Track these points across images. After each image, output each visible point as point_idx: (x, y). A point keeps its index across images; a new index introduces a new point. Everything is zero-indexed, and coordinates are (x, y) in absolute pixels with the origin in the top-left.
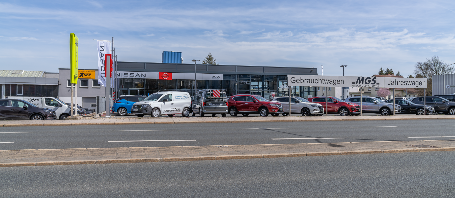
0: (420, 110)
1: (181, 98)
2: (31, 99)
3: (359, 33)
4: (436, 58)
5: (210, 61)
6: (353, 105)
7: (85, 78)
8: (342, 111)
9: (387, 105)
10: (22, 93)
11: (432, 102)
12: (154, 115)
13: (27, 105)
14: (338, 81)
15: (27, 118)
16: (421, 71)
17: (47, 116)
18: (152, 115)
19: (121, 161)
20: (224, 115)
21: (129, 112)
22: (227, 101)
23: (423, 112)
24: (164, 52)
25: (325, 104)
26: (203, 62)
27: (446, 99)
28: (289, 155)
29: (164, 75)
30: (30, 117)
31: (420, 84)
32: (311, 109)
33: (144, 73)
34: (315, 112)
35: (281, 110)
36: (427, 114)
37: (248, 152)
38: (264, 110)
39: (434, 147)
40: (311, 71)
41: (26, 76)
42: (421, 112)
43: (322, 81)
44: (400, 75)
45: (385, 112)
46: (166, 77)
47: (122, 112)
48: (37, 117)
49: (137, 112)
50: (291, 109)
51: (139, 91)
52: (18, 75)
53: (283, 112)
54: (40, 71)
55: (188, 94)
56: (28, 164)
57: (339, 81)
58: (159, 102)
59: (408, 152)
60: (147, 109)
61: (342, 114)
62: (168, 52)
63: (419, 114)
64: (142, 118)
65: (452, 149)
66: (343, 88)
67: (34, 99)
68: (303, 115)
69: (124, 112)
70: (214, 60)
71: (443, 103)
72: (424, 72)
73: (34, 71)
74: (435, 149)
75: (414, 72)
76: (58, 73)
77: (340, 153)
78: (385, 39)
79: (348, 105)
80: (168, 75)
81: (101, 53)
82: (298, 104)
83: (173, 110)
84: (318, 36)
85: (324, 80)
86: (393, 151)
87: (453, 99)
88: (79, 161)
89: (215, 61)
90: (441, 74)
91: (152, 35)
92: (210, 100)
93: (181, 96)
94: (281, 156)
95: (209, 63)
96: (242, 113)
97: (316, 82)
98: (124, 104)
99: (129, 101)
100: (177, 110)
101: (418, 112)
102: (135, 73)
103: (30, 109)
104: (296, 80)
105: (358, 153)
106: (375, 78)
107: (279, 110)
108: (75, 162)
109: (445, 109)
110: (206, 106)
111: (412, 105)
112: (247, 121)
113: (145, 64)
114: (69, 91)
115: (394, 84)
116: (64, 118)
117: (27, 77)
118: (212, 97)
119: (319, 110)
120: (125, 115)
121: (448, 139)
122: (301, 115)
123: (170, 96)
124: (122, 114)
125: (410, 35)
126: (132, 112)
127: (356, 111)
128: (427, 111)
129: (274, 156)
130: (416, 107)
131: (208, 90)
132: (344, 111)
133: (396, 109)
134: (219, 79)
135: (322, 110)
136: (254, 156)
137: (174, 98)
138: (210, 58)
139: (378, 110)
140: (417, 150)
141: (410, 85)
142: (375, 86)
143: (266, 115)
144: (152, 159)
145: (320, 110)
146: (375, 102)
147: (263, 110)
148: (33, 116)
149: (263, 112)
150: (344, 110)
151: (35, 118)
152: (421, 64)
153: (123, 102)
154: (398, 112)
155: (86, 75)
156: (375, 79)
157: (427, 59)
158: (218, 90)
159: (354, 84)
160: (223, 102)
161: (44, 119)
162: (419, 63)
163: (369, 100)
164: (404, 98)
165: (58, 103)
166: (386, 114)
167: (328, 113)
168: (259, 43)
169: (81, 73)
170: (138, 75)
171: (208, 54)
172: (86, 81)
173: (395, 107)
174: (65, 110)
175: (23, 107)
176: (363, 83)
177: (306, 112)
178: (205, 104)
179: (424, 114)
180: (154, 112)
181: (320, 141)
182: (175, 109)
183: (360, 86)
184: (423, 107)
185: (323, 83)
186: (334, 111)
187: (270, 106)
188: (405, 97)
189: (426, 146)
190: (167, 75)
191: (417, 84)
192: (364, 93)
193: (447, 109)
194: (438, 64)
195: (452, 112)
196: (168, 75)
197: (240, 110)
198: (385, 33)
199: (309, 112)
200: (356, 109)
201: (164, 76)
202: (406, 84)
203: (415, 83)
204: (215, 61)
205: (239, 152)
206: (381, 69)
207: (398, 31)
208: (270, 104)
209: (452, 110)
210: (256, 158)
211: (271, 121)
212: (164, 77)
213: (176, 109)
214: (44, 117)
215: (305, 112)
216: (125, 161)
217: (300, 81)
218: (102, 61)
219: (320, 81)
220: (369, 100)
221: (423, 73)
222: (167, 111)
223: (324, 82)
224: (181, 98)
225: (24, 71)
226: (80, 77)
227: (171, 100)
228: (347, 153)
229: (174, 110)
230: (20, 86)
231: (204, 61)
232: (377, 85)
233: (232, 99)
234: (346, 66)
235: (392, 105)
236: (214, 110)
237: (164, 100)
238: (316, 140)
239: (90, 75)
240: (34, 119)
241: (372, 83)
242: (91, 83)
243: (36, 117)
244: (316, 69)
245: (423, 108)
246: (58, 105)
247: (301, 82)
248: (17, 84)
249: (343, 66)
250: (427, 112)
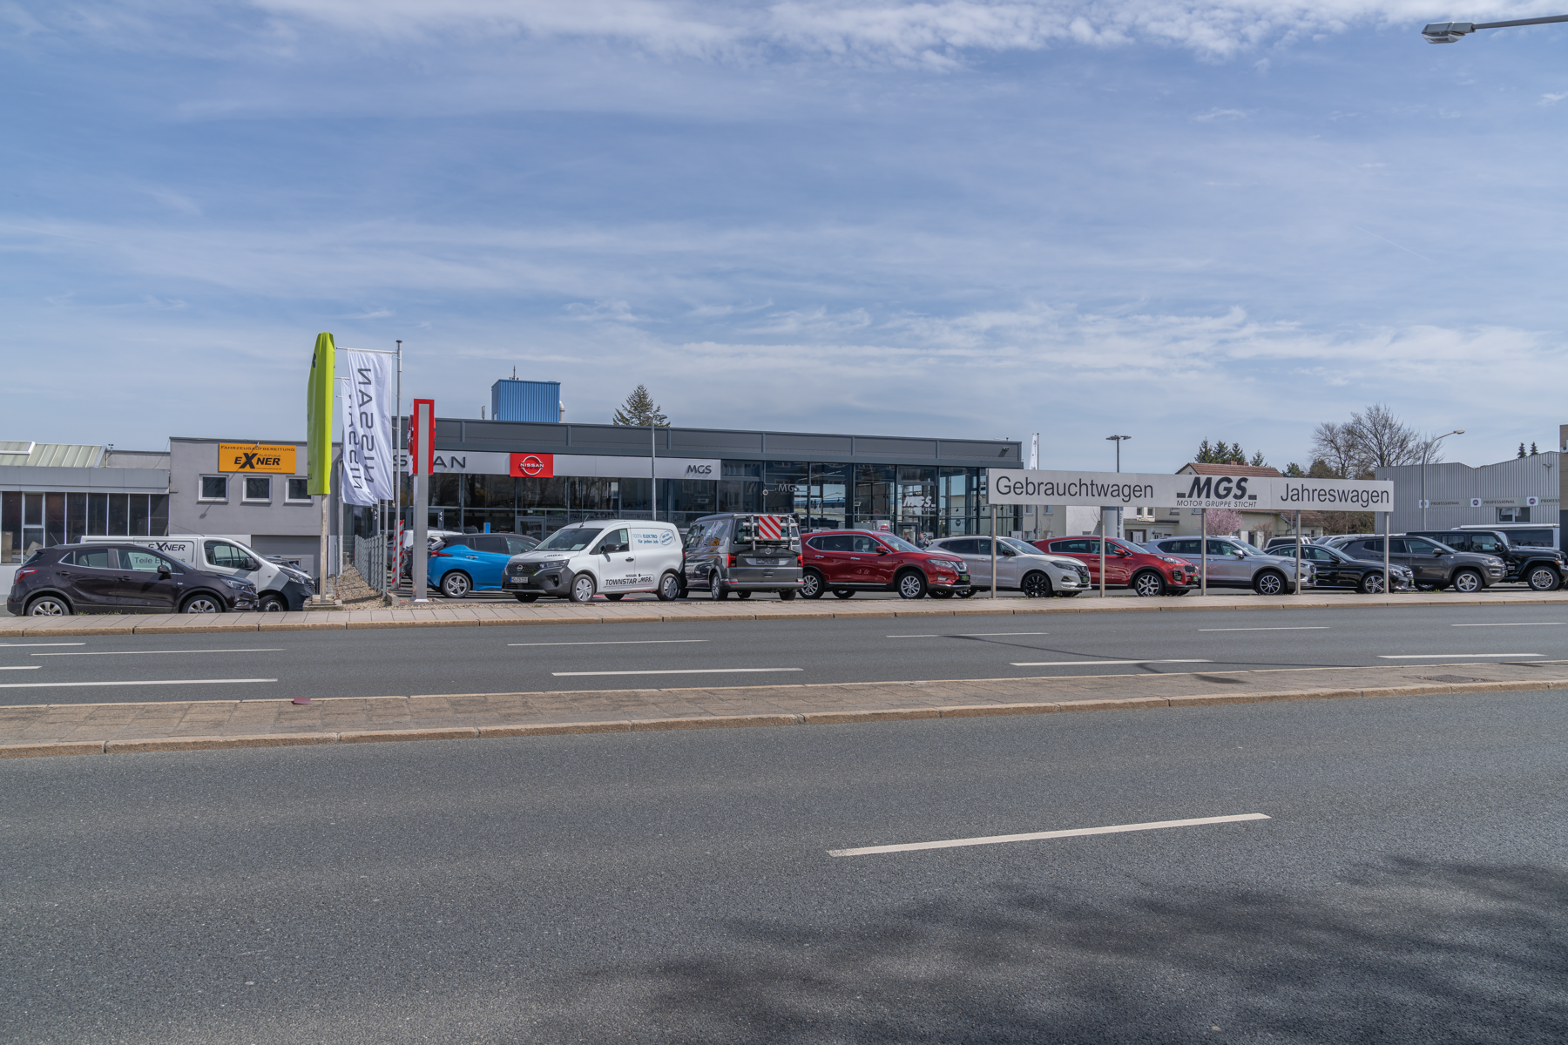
0: (1372, 577)
1: (655, 539)
2: (158, 544)
3: (1091, 317)
4: (1382, 411)
5: (640, 412)
6: (1178, 562)
7: (260, 470)
8: (1143, 582)
9: (1277, 562)
10: (40, 523)
11: (1404, 555)
12: (579, 594)
13: (168, 565)
14: (1136, 489)
15: (170, 605)
16: (1334, 451)
17: (233, 598)
18: (569, 596)
19: (697, 722)
20: (787, 595)
21: (478, 584)
22: (801, 552)
23: (1382, 584)
24: (500, 381)
25: (1097, 560)
26: (619, 416)
27: (1441, 542)
28: (1125, 703)
29: (526, 462)
30: (179, 602)
31: (1137, 494)
32: (1056, 576)
33: (459, 455)
34: (1066, 586)
35: (965, 578)
36: (1392, 591)
37: (1016, 697)
38: (912, 579)
39: (1484, 680)
40: (1004, 451)
41: (43, 463)
42: (1375, 585)
43: (1090, 487)
44: (1263, 464)
45: (1270, 586)
46: (531, 467)
47: (457, 585)
48: (202, 604)
49: (524, 586)
50: (997, 575)
51: (441, 514)
52: (14, 459)
53: (969, 586)
54: (92, 447)
55: (672, 526)
56: (456, 733)
57: (1020, 486)
58: (592, 553)
59: (1424, 695)
60: (557, 576)
61: (1143, 590)
62: (541, 383)
63: (1368, 590)
64: (532, 605)
65: (1534, 685)
66: (1103, 508)
67: (169, 544)
68: (1030, 596)
69: (462, 585)
70: (655, 408)
71: (1437, 556)
72: (1343, 456)
73: (69, 446)
74: (1492, 686)
75: (1311, 454)
76: (168, 454)
77: (1254, 698)
78: (1176, 339)
79: (1163, 562)
80: (539, 464)
81: (360, 391)
82: (1011, 559)
83: (633, 578)
84: (956, 328)
85: (1094, 487)
86: (1385, 691)
87: (1463, 544)
88: (589, 724)
89: (658, 411)
90: (1394, 465)
91: (384, 313)
92: (751, 549)
93: (654, 536)
94: (1105, 706)
95: (639, 419)
96: (835, 590)
97: (1073, 492)
98: (462, 559)
99: (478, 550)
100: (642, 579)
101: (1367, 585)
103: (178, 579)
104: (1012, 484)
105: (1298, 697)
106: (1245, 480)
107: (957, 578)
108: (579, 727)
109: (1443, 576)
110: (738, 568)
111: (1348, 562)
112: (880, 614)
113: (464, 424)
114: (203, 516)
115: (1298, 499)
116: (269, 605)
117: (45, 465)
118: (757, 538)
119: (1078, 577)
120: (463, 597)
121: (1503, 662)
122: (1023, 594)
123: (622, 534)
124: (456, 593)
125: (1251, 329)
126: (503, 587)
127: (1187, 580)
128: (1394, 580)
129: (1087, 706)
130: (1359, 570)
131: (744, 515)
132: (1149, 582)
133: (1303, 576)
134: (710, 477)
135: (1085, 579)
136: (1036, 707)
137: (633, 542)
138: (640, 402)
139: (1249, 578)
140: (1445, 690)
141: (1346, 501)
142: (1243, 504)
143: (920, 596)
144: (778, 718)
145: (1081, 578)
146: (1241, 552)
147: (909, 577)
148: (189, 601)
149: (910, 586)
150: (1150, 578)
151: (195, 606)
152: (1333, 429)
153: (459, 555)
154: (1308, 584)
155: (265, 461)
156: (1243, 484)
157: (1354, 415)
158: (775, 516)
159: (1183, 499)
160: (790, 553)
161: (224, 610)
162: (1327, 427)
163: (1216, 547)
164: (1306, 541)
165: (251, 557)
166: (1272, 591)
167: (1107, 588)
168: (763, 348)
169: (246, 455)
171: (636, 389)
172: (262, 480)
173: (1300, 570)
174: (271, 579)
175: (159, 571)
176: (1208, 496)
177: (1039, 586)
178: (733, 561)
179: (1382, 589)
180: (578, 587)
181: (1153, 668)
182: (637, 577)
183: (1201, 503)
184: (1383, 568)
185: (1093, 495)
186: (1120, 581)
187: (933, 566)
188: (1306, 538)
189: (1461, 679)
190: (537, 462)
191: (1365, 499)
192: (1156, 521)
193: (1447, 575)
194: (1387, 431)
195: (1462, 585)
196: (539, 464)
197: (832, 579)
198: (1173, 319)
199: (1048, 583)
200: (1187, 574)
201: (529, 465)
202: (1332, 498)
203: (1118, 490)
204: (658, 411)
205: (979, 698)
206: (1205, 443)
207: (1216, 315)
208: (933, 561)
209: (1462, 577)
210: (1043, 712)
211: (951, 612)
212: (526, 468)
213: (640, 575)
214: (226, 604)
215: (1036, 584)
216: (708, 722)
217: (1024, 490)
218: (364, 416)
219: (1084, 488)
220: (1216, 547)
221: (1340, 458)
222: (615, 582)
223: (1095, 492)
224: (655, 539)
225: (33, 444)
226: (243, 466)
227: (625, 548)
228: (1272, 698)
229: (635, 581)
230: (34, 498)
231: (620, 414)
232: (1251, 501)
233: (807, 543)
234: (1125, 438)
235: (1291, 564)
236: (760, 578)
237: (605, 548)
238: (1141, 666)
239: (279, 460)
240: (191, 608)
242: (280, 488)
243: (198, 603)
244: (1018, 444)
245: (1382, 574)
246: (250, 564)
247: (1027, 493)
248: (23, 489)
249: (1116, 438)
250: (1392, 584)
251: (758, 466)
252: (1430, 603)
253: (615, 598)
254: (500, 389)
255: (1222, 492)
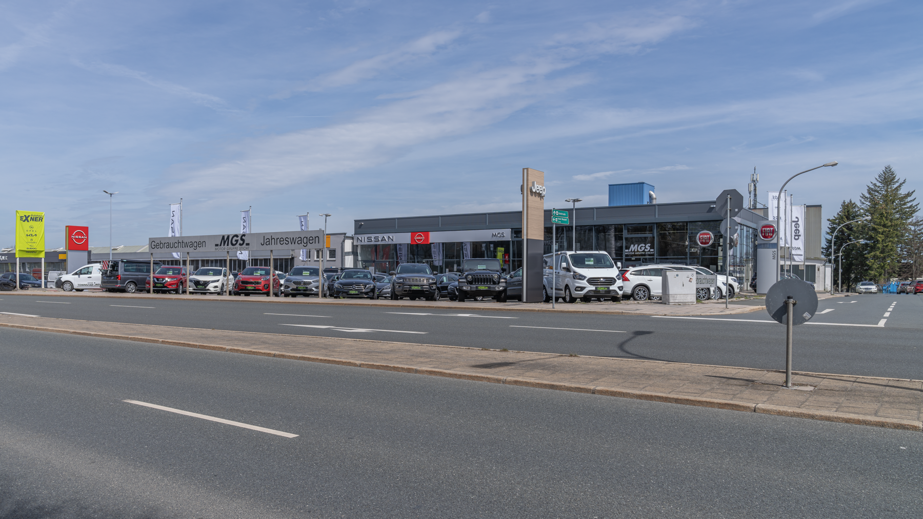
31: (200, 245)
33: (391, 235)
102: (380, 236)
104: (155, 244)
115: (269, 244)
141: (295, 243)
156: (243, 237)
170: (383, 239)
176: (228, 245)
182: (94, 284)
191: (305, 242)
202: (287, 243)
222: (82, 285)
223: (184, 246)
230: (261, 260)
241: (240, 245)
244: (356, 221)
251: (652, 226)
252: (582, 312)
253: (78, 290)
254: (614, 189)
255: (234, 242)
